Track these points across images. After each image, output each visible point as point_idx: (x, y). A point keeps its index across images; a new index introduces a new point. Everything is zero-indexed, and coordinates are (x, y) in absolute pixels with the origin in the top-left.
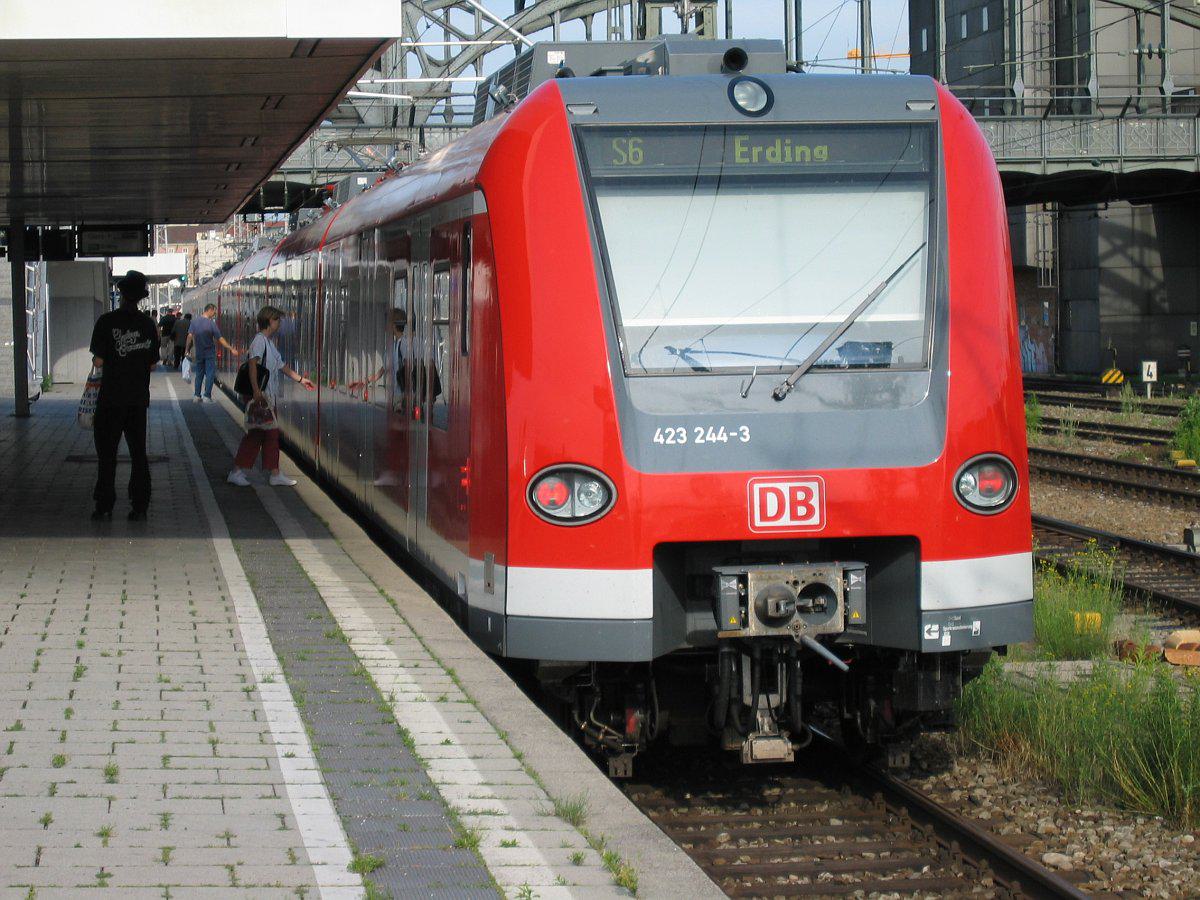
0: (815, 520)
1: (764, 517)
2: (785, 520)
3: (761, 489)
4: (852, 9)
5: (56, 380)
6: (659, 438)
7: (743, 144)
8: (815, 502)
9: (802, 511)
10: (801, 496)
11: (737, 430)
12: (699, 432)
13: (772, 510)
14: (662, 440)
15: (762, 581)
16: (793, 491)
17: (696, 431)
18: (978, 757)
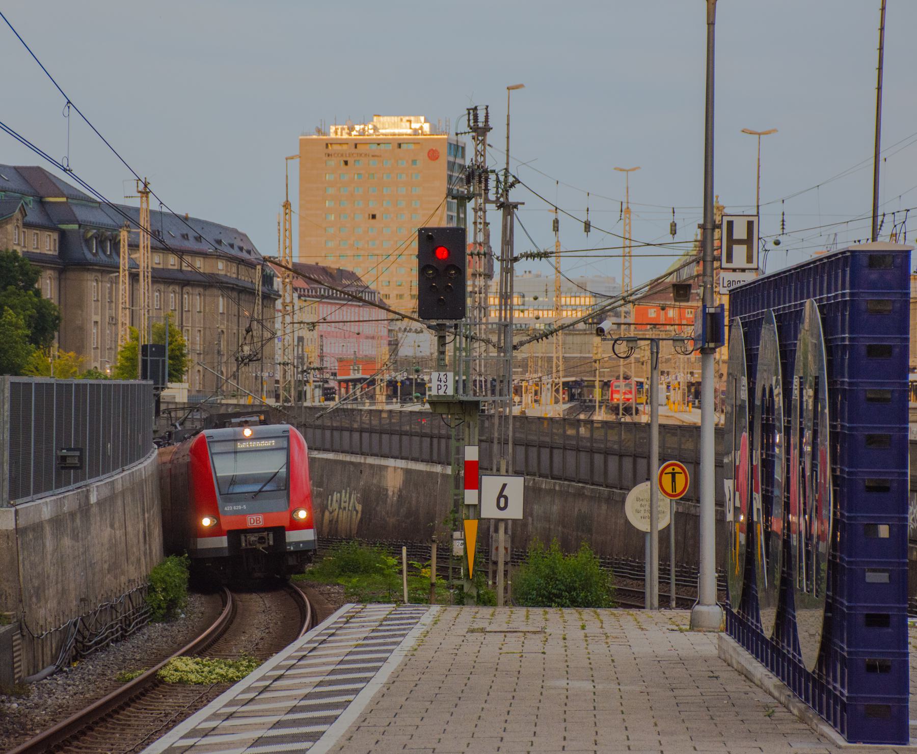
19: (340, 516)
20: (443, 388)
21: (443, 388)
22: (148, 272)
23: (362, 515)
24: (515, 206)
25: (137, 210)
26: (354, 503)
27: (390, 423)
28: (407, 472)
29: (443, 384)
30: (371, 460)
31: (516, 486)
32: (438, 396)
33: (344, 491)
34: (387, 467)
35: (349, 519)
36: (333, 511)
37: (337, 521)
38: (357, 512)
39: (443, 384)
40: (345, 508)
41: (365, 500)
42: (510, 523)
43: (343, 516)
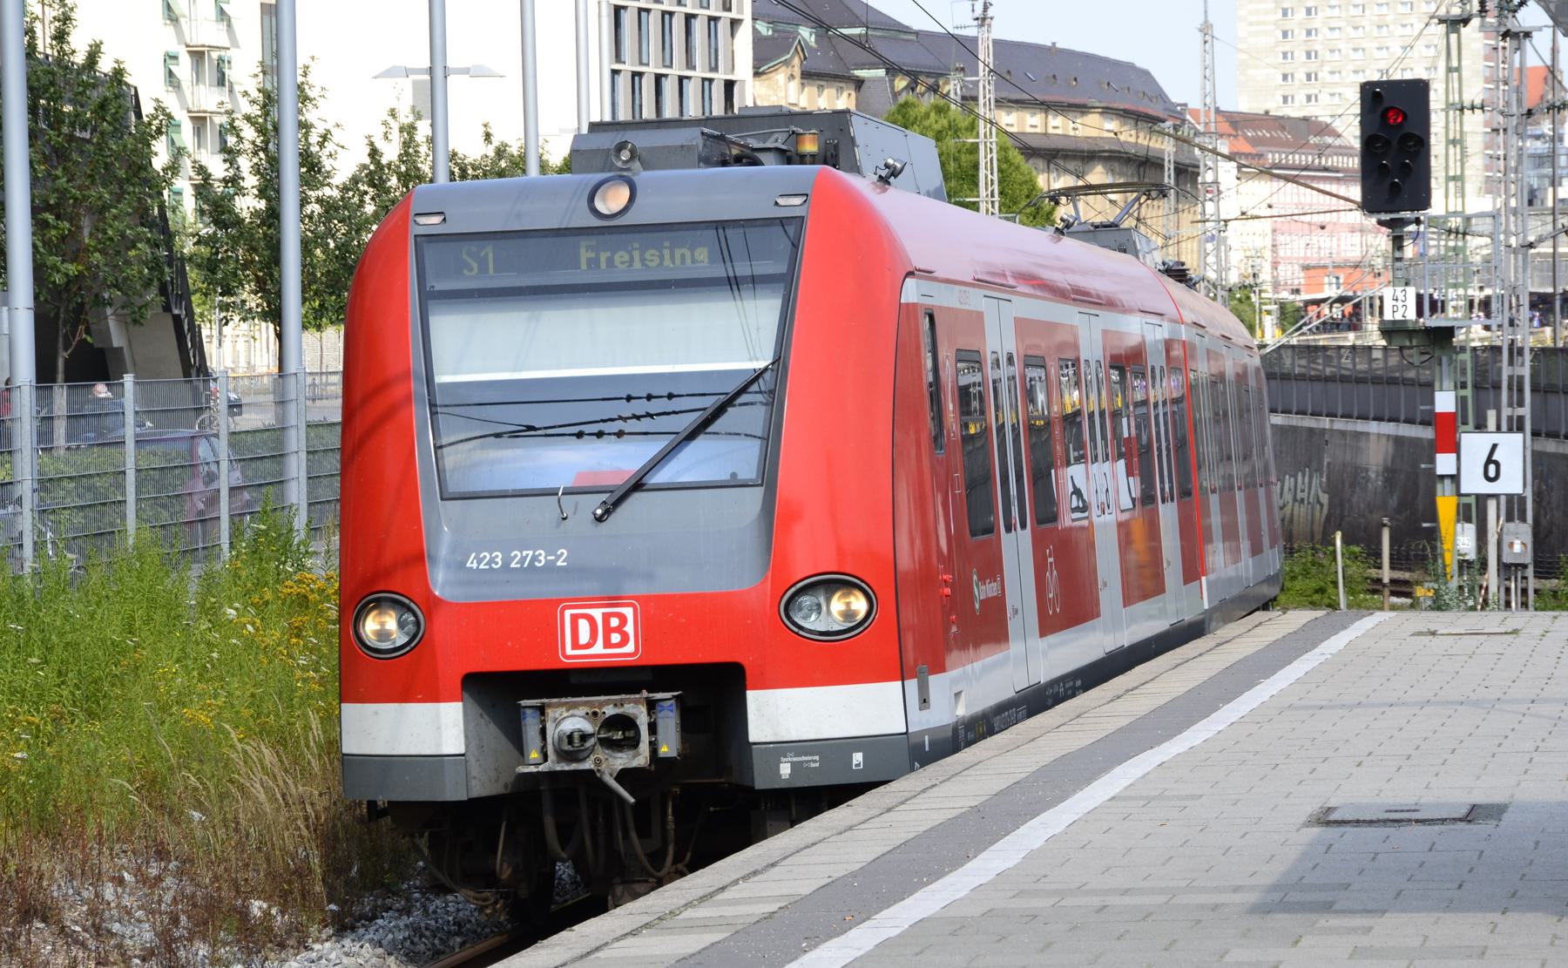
0: (630, 648)
1: (576, 645)
2: (598, 648)
3: (572, 615)
4: (1203, 4)
5: (758, 442)
6: (472, 563)
7: (588, 248)
8: (629, 628)
9: (616, 638)
10: (614, 622)
11: (555, 554)
12: (562, 554)
13: (584, 637)
14: (475, 566)
15: (570, 719)
16: (606, 617)
17: (512, 555)
18: (237, 934)
19: (1296, 513)
20: (1401, 310)
21: (1401, 310)
22: (991, 143)
23: (1329, 509)
24: (1527, 35)
25: (975, 40)
26: (1317, 491)
27: (1386, 368)
28: (1398, 441)
29: (1400, 304)
30: (1340, 424)
31: (1513, 450)
32: (1394, 322)
33: (1300, 474)
34: (1368, 434)
35: (1309, 517)
36: (1284, 506)
37: (1291, 521)
38: (1322, 505)
39: (1400, 304)
40: (1302, 500)
41: (1333, 489)
42: (1503, 500)
43: (1301, 512)
